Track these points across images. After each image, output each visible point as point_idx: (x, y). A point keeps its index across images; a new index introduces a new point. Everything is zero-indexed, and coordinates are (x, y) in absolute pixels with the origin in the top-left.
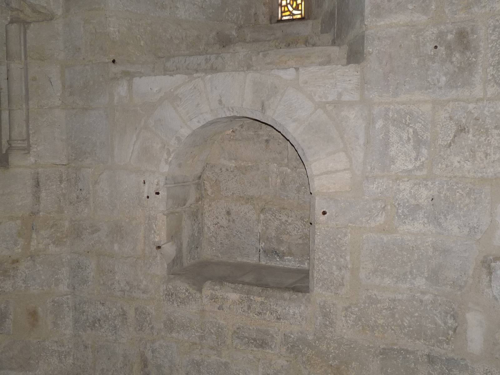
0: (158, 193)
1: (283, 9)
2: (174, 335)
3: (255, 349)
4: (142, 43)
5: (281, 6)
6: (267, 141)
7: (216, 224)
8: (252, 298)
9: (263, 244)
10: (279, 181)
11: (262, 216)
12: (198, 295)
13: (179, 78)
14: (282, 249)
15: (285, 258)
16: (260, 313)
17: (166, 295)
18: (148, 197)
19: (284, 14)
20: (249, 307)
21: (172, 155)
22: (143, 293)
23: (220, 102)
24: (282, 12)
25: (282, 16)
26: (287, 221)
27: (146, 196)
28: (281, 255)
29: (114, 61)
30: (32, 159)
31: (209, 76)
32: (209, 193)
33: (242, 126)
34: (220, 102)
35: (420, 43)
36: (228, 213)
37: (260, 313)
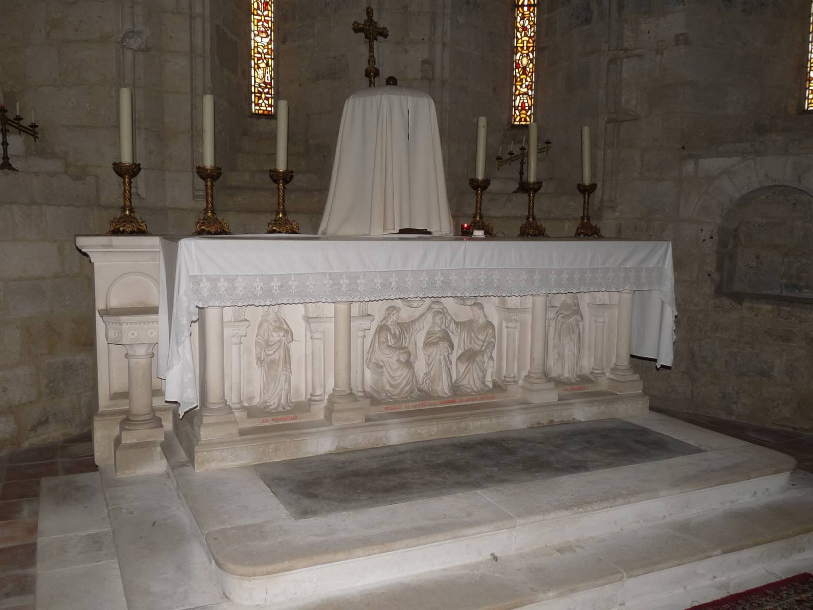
0: (712, 238)
1: (810, 101)
2: (718, 335)
3: (781, 343)
4: (702, 134)
5: (808, 99)
6: (794, 204)
7: (747, 265)
8: (781, 308)
9: (786, 280)
10: (802, 233)
11: (786, 260)
12: (739, 307)
13: (735, 159)
14: (801, 284)
15: (804, 290)
16: (787, 319)
17: (714, 307)
18: (704, 240)
19: (810, 105)
20: (779, 315)
21: (725, 211)
22: (696, 306)
23: (766, 175)
24: (808, 104)
25: (808, 107)
26: (806, 263)
27: (703, 239)
28: (800, 289)
29: (683, 148)
30: (617, 214)
31: (758, 158)
32: (743, 242)
33: (774, 193)
34: (766, 175)
35: (599, 296)
36: (758, 257)
37: (787, 319)
